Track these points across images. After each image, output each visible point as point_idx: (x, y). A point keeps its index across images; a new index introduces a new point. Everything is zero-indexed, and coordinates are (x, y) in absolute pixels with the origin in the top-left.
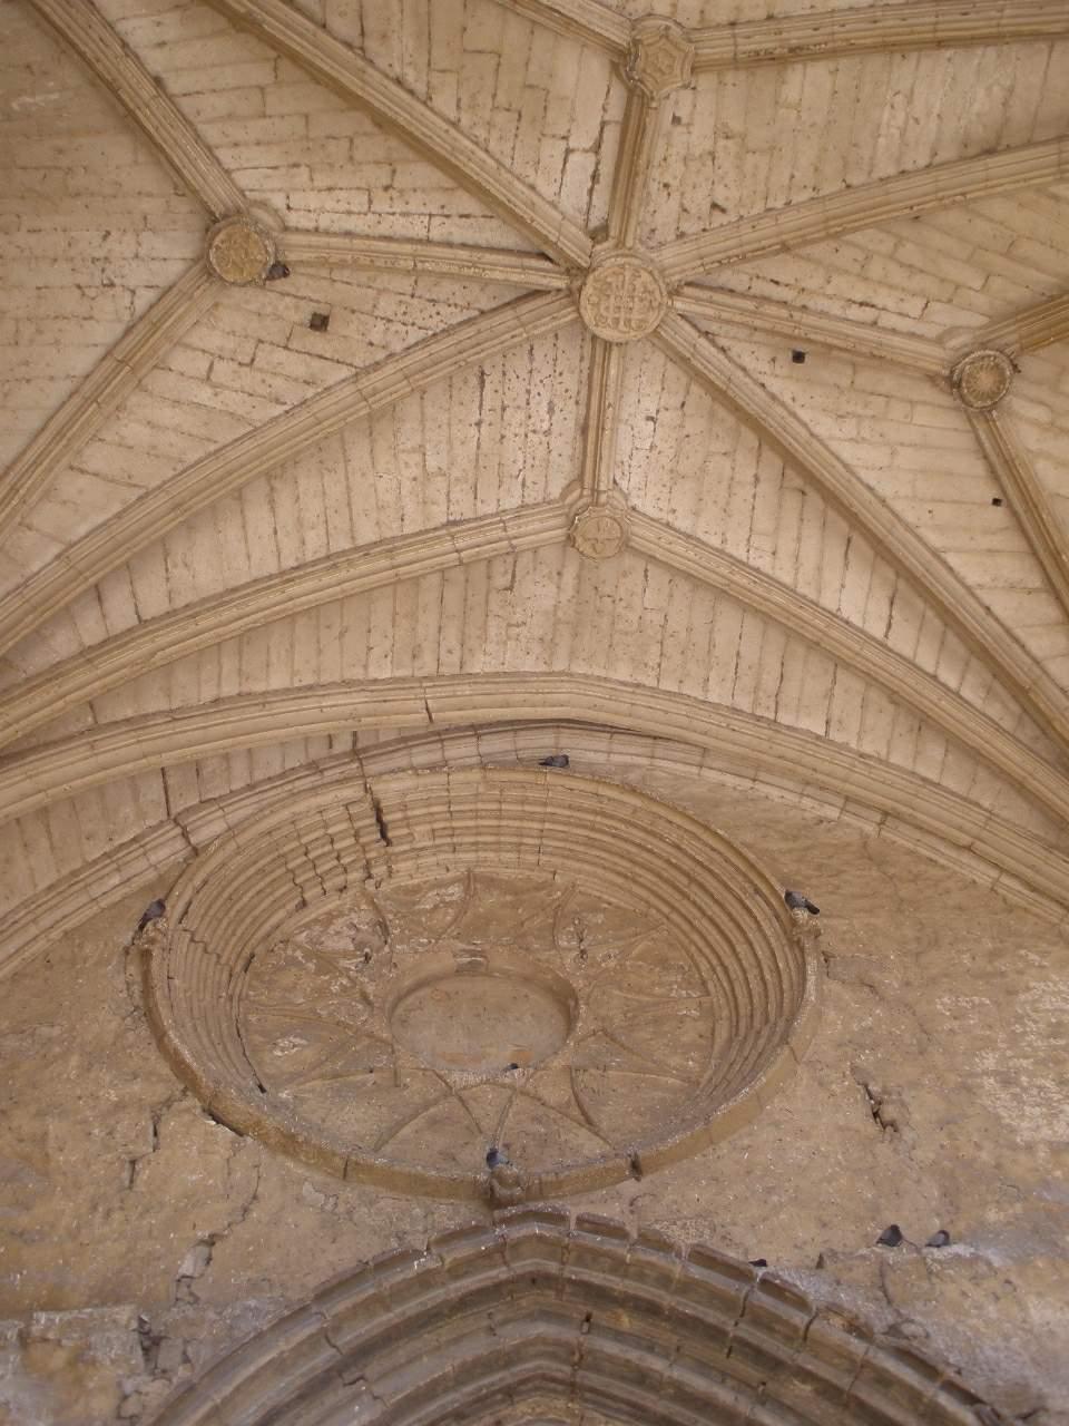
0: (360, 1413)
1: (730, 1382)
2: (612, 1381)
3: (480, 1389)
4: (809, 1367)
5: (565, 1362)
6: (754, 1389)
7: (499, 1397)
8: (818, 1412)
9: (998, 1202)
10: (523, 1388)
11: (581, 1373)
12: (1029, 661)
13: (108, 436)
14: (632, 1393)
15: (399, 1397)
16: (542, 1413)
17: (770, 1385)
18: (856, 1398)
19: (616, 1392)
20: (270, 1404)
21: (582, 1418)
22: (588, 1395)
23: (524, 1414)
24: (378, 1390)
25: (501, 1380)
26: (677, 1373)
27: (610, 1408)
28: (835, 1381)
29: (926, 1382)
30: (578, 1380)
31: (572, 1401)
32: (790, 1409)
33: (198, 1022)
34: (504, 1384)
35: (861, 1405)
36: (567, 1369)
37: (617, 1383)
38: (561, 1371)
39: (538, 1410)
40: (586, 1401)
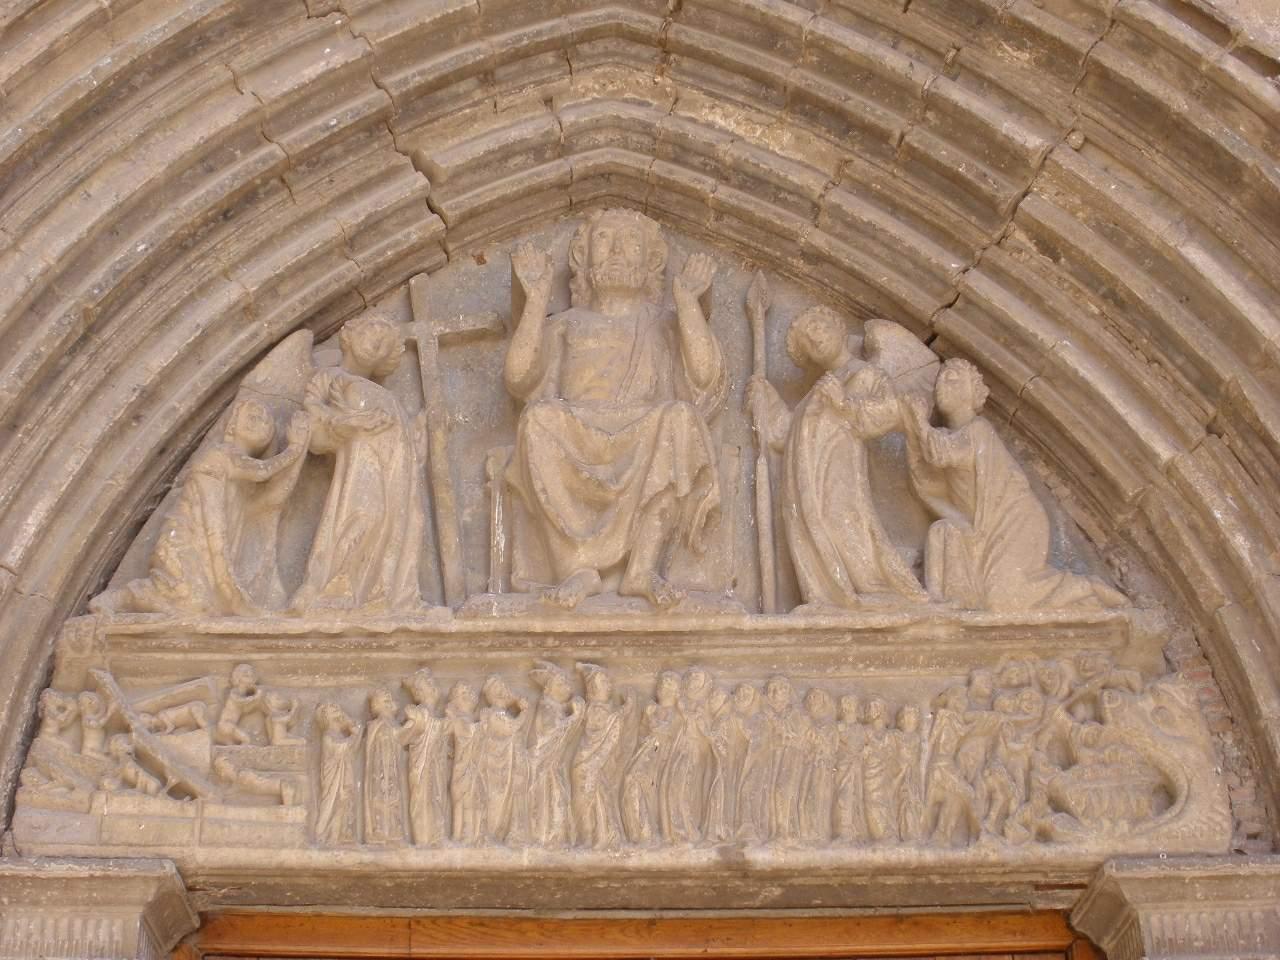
0: (331, 54)
1: (905, 46)
2: (722, 39)
3: (520, 39)
4: (1030, 19)
5: (655, 12)
6: (940, 55)
7: (550, 58)
8: (1037, 91)
9: (1012, 658)
10: (585, 48)
11: (675, 26)
12: (1105, 131)
13: (403, 140)
14: (750, 55)
15: (391, 35)
16: (614, 93)
17: (965, 52)
18: (1099, 65)
19: (728, 55)
20: (187, 21)
21: (676, 100)
22: (687, 64)
23: (588, 90)
24: (359, 26)
25: (552, 29)
26: (824, 28)
27: (712, 81)
28: (1066, 39)
29: (1210, 44)
30: (671, 35)
31: (662, 74)
32: (991, 82)
33: (368, 297)
34: (556, 34)
35: (1104, 75)
36: (656, 21)
37: (729, 42)
38: (647, 22)
39: (610, 87)
40: (683, 72)
